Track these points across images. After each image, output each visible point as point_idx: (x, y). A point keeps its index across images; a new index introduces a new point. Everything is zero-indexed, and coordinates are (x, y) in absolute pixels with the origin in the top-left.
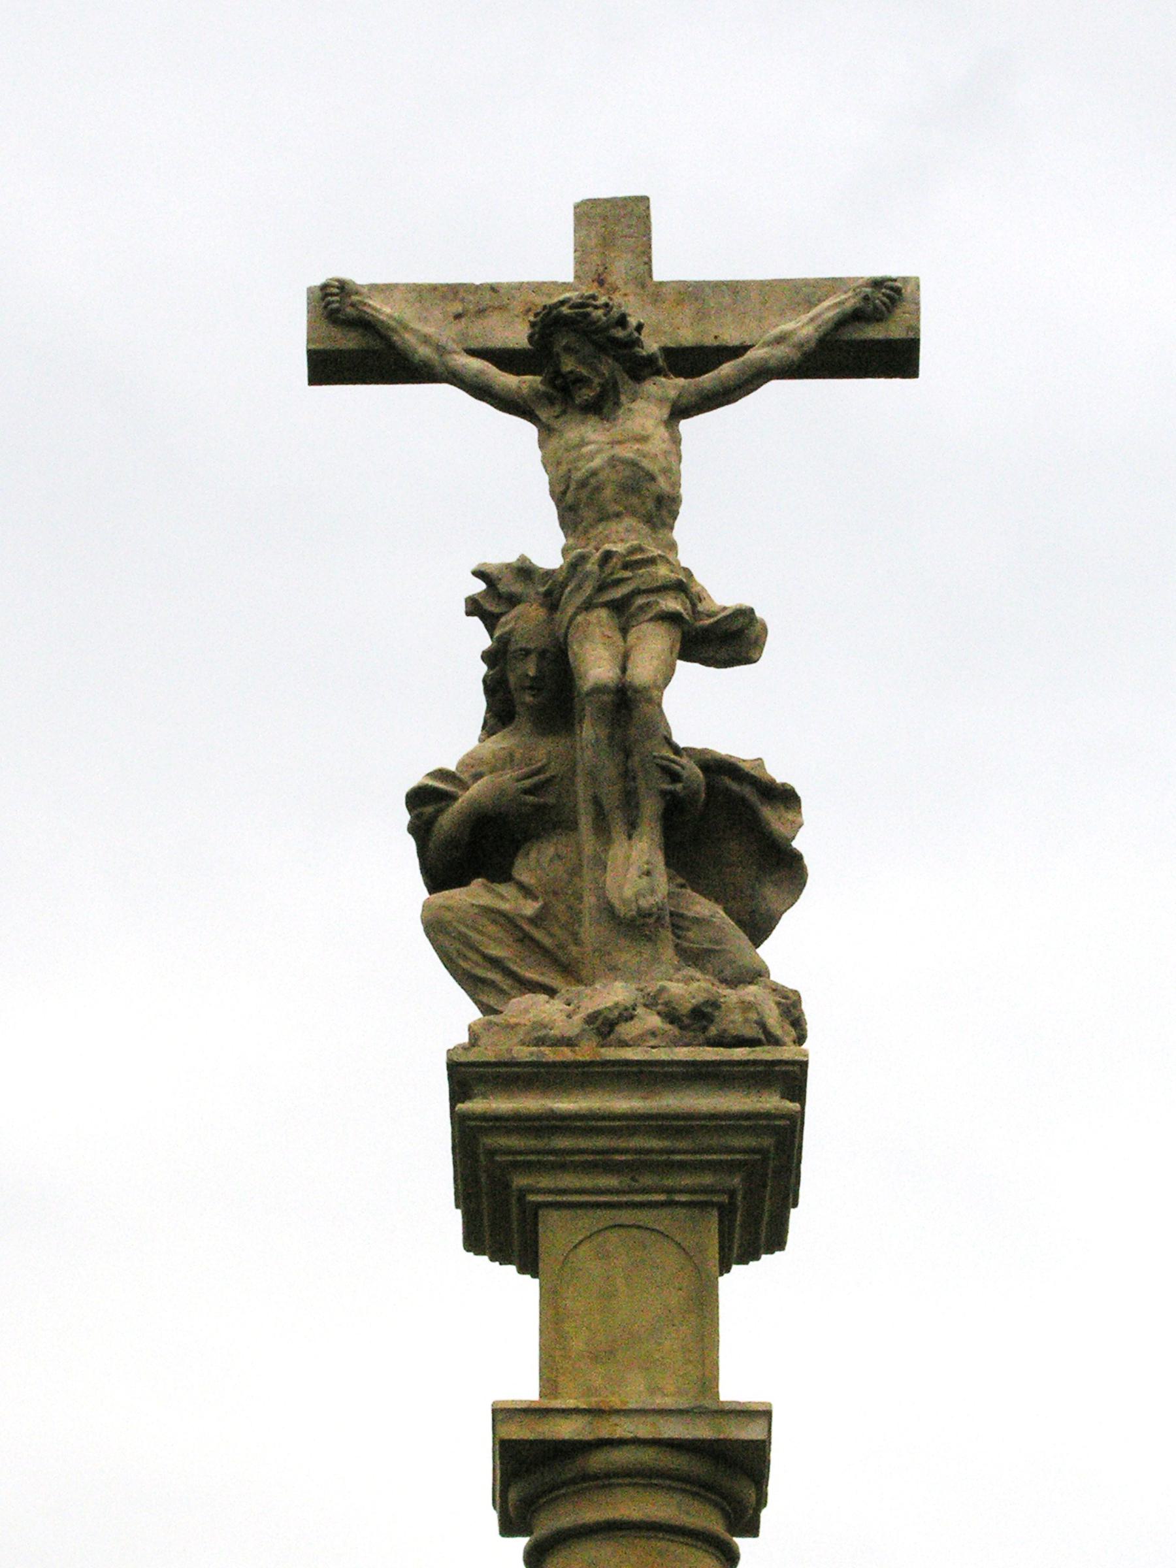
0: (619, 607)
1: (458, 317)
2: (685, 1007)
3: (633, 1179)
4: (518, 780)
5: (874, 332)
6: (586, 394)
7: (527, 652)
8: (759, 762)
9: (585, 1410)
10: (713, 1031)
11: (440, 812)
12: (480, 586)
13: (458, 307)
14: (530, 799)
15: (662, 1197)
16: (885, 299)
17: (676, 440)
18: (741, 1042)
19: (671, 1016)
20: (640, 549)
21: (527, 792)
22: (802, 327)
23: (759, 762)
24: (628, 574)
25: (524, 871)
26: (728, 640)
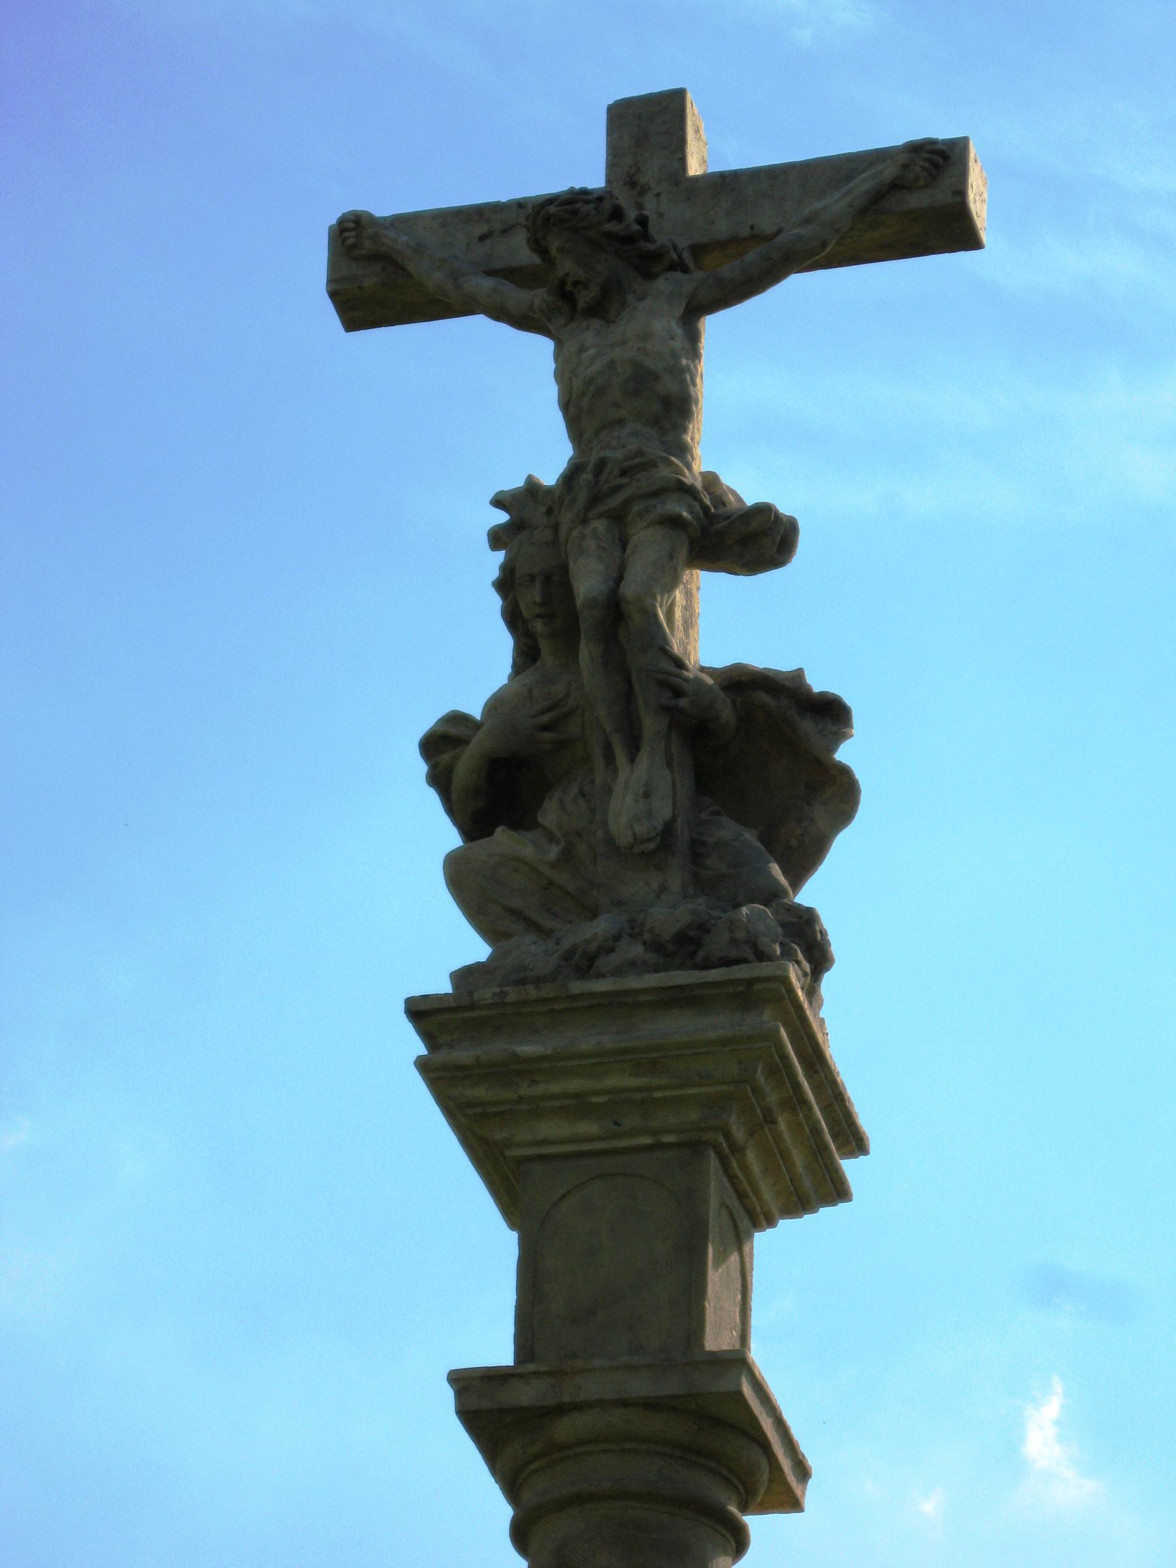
0: (618, 518)
1: (482, 238)
2: (668, 931)
3: (616, 1123)
4: (534, 717)
5: (917, 200)
6: (584, 298)
7: (532, 578)
8: (799, 674)
9: (546, 1372)
10: (701, 955)
11: (455, 759)
12: (502, 517)
13: (483, 229)
14: (547, 735)
15: (648, 1141)
16: (927, 165)
17: (693, 337)
18: (728, 962)
19: (655, 946)
20: (640, 453)
21: (546, 728)
22: (836, 204)
23: (799, 674)
24: (625, 480)
25: (550, 815)
26: (755, 540)
